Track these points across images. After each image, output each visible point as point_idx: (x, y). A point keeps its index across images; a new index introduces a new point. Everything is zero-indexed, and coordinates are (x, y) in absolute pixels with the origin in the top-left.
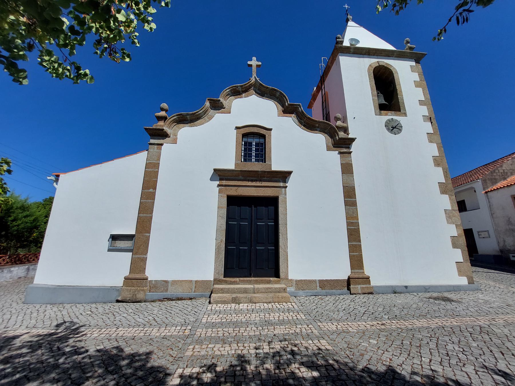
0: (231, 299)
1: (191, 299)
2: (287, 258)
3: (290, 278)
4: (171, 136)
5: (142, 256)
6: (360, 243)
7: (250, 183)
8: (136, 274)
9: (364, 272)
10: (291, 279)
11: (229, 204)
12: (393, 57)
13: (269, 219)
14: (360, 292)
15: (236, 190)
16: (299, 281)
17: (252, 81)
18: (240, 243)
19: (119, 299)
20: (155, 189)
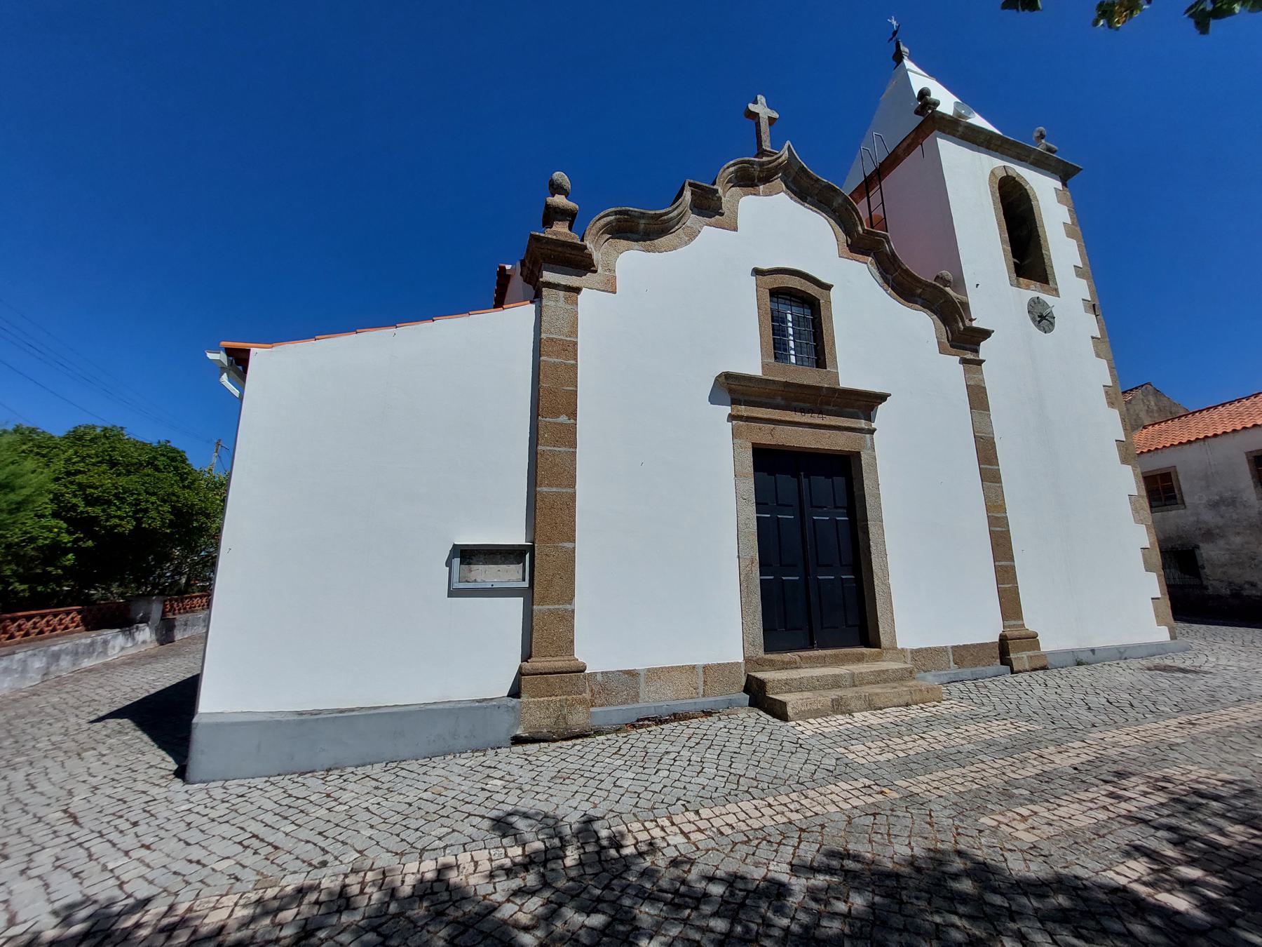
0: (829, 704)
1: (708, 714)
2: (891, 599)
3: (899, 646)
4: (599, 271)
5: (561, 606)
7: (798, 417)
8: (551, 659)
10: (903, 649)
11: (758, 467)
13: (836, 507)
14: (1027, 667)
15: (771, 432)
17: (783, 158)
18: (781, 565)
19: (520, 732)
20: (573, 415)
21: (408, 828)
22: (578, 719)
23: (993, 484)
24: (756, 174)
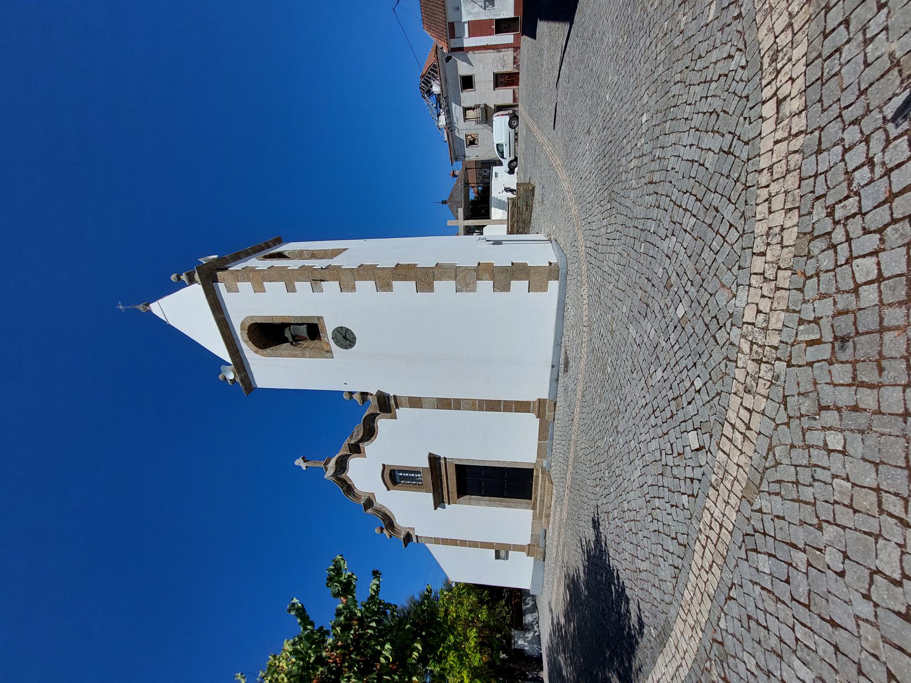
6: (502, 402)
9: (534, 402)
12: (225, 318)
14: (553, 414)
16: (538, 455)
21: (702, 558)
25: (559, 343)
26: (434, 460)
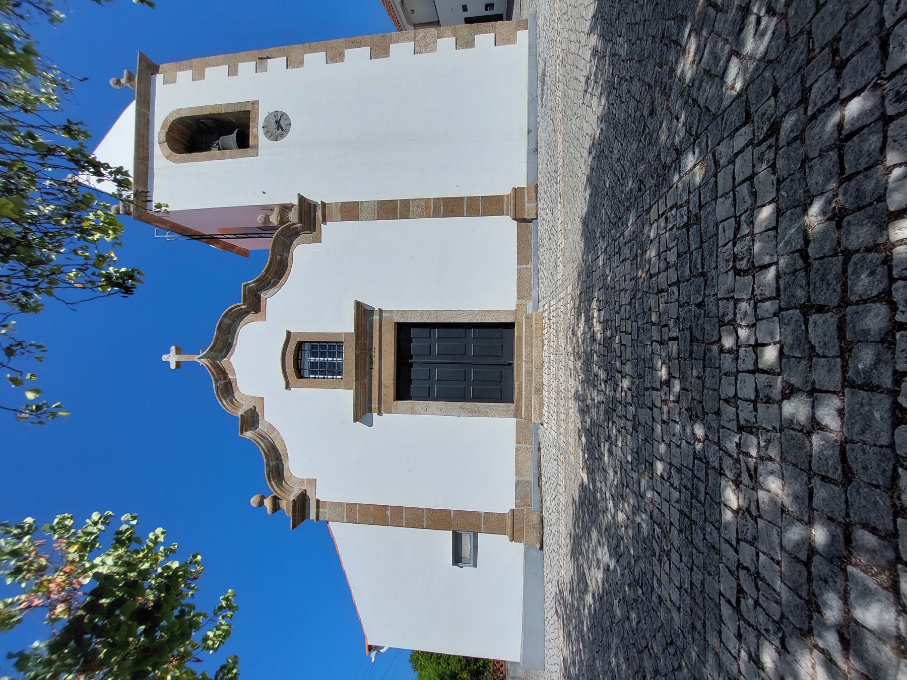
3: (514, 308)
6: (465, 199)
7: (376, 366)
11: (409, 398)
14: (534, 205)
16: (518, 295)
19: (538, 546)
20: (386, 507)
22: (535, 518)
23: (411, 209)
24: (222, 382)
25: (535, 97)
26: (363, 313)
